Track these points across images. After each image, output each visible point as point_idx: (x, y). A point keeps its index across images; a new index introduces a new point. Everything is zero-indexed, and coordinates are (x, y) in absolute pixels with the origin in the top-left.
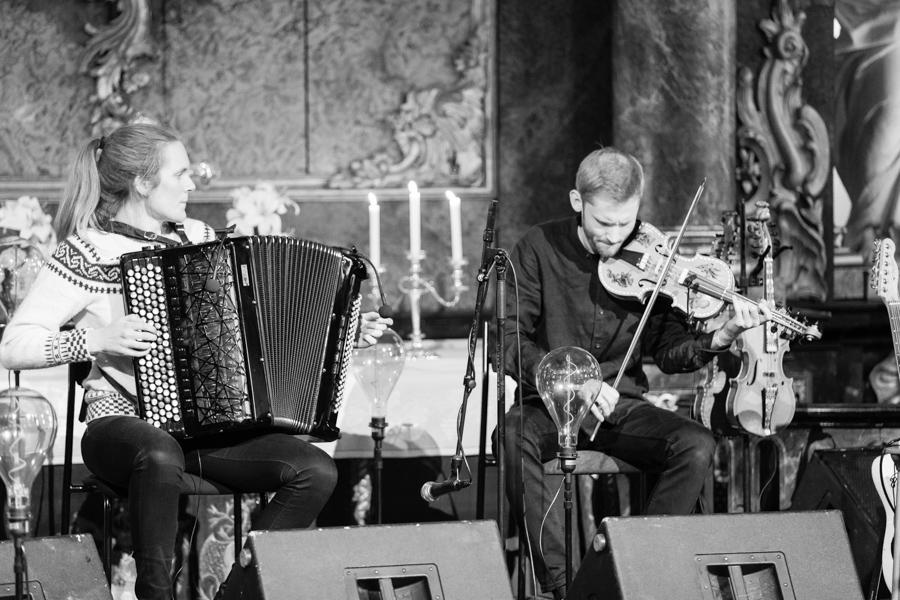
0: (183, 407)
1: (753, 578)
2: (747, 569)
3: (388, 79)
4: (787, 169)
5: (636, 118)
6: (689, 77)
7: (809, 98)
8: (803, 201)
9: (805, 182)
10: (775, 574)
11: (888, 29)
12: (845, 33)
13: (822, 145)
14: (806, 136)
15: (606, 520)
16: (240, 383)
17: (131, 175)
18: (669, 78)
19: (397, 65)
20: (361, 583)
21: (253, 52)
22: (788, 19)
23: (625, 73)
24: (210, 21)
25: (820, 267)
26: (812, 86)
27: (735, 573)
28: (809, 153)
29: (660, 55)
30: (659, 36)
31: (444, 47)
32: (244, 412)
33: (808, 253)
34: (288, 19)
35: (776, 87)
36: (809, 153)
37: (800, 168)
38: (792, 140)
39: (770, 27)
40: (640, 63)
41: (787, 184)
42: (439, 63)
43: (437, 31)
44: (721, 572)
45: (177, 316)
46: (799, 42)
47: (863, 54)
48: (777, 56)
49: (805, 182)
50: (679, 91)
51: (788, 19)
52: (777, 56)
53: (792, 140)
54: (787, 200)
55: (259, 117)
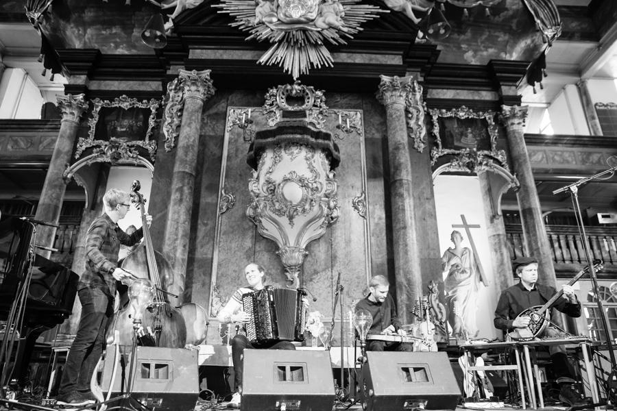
0: (257, 335)
1: (418, 373)
2: (416, 370)
3: (349, 297)
4: (437, 316)
5: (402, 301)
6: (412, 291)
7: (440, 301)
8: (441, 323)
9: (441, 319)
10: (425, 371)
11: (456, 291)
12: (447, 293)
13: (444, 311)
14: (440, 309)
15: (367, 352)
16: (270, 328)
17: (62, 113)
18: (408, 292)
19: (351, 294)
20: (279, 367)
21: (321, 291)
22: (434, 285)
23: (398, 292)
24: (312, 285)
25: (447, 338)
26: (441, 298)
27: (411, 370)
28: (441, 312)
29: (406, 287)
30: (405, 283)
31: (362, 291)
32: (271, 336)
33: (444, 335)
34: (328, 285)
35: (433, 299)
36: (441, 312)
37: (440, 316)
38: (437, 310)
39: (430, 287)
40: (401, 289)
41: (437, 320)
42: (360, 294)
43: (359, 287)
44: (406, 370)
45: (255, 312)
46: (437, 290)
47: (452, 297)
48: (433, 292)
49: (441, 319)
50: (410, 294)
51: (434, 285)
52: (433, 292)
53: (437, 310)
54: (438, 323)
55: (322, 304)
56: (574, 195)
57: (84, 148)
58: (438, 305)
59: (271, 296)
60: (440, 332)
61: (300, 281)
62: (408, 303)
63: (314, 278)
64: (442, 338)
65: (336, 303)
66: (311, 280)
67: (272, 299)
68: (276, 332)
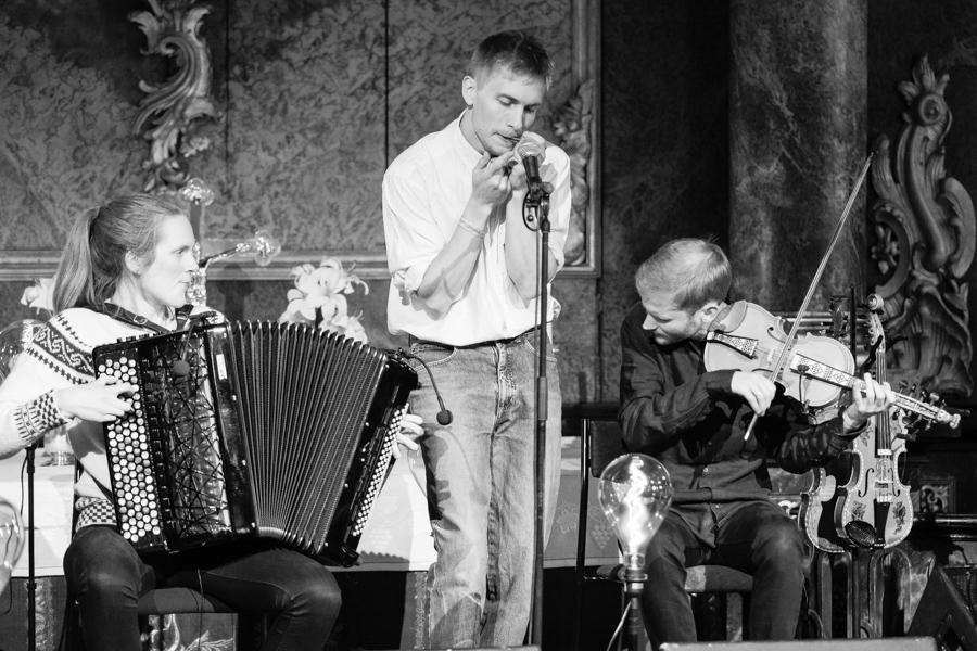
0: (163, 518)
4: (928, 246)
8: (946, 285)
9: (949, 263)
21: (327, 113)
22: (929, 79)
24: (279, 78)
28: (954, 232)
35: (917, 156)
36: (954, 232)
37: (943, 248)
39: (910, 89)
41: (928, 264)
46: (942, 107)
49: (949, 263)
50: (802, 160)
51: (929, 79)
55: (333, 185)
56: (744, 508)
57: (50, 237)
58: (940, 187)
59: (220, 359)
60: (937, 328)
61: (212, 60)
62: (788, 203)
63: (291, 41)
64: (944, 360)
65: (409, 235)
66: (273, 51)
67: (223, 374)
68: (241, 505)
